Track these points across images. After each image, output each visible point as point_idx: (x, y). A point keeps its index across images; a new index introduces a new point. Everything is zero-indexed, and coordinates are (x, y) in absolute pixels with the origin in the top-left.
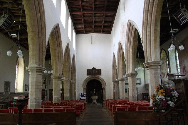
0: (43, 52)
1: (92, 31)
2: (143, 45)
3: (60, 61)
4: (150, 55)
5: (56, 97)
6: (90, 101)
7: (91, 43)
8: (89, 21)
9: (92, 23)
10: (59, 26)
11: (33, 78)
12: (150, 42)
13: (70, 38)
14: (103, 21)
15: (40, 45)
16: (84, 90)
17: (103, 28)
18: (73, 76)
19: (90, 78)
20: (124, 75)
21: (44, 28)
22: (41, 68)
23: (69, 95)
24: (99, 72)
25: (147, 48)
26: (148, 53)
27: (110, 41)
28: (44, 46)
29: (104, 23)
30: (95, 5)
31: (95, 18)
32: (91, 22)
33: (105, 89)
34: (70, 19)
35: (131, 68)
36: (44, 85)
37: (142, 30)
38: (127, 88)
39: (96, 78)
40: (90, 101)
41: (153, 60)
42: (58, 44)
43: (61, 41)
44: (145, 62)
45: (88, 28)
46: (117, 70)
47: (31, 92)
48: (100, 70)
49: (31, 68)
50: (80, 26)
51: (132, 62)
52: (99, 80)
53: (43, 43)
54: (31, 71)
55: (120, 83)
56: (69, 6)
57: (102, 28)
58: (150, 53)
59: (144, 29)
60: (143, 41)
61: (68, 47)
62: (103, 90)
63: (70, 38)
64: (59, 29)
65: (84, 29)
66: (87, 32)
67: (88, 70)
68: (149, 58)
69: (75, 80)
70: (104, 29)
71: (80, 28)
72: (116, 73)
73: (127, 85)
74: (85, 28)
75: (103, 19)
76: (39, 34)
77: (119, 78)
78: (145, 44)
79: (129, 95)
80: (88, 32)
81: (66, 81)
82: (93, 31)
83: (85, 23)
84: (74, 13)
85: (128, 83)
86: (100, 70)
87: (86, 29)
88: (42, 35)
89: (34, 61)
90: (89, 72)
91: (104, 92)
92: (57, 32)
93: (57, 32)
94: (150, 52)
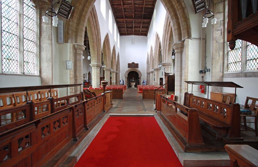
1: (132, 34)
3: (109, 58)
6: (130, 86)
7: (132, 44)
8: (130, 26)
9: (133, 27)
13: (116, 41)
16: (126, 78)
17: (141, 31)
18: (118, 68)
19: (130, 70)
20: (159, 65)
23: (115, 81)
24: (136, 65)
27: (146, 41)
29: (142, 28)
30: (134, 14)
33: (141, 78)
34: (115, 24)
39: (135, 70)
41: (166, 62)
42: (108, 47)
44: (162, 63)
45: (129, 31)
48: (138, 64)
50: (123, 29)
52: (137, 71)
55: (151, 74)
56: (114, 15)
60: (162, 49)
62: (140, 79)
63: (116, 41)
65: (126, 32)
66: (129, 34)
67: (129, 64)
68: (164, 60)
69: (119, 71)
71: (124, 30)
72: (148, 68)
74: (127, 31)
81: (107, 70)
82: (133, 34)
83: (127, 27)
84: (118, 20)
86: (138, 64)
87: (128, 32)
89: (95, 60)
90: (130, 65)
91: (140, 80)
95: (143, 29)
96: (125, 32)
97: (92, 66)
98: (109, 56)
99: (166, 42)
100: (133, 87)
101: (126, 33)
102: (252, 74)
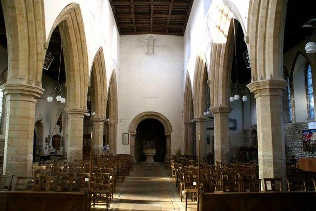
0: (37, 54)
2: (248, 46)
3: (82, 79)
4: (262, 67)
5: (72, 149)
6: (142, 158)
8: (145, 9)
10: (80, 10)
11: (224, 160)
12: (265, 38)
14: (170, 10)
15: (31, 40)
17: (170, 24)
20: (206, 111)
21: (38, 2)
22: (32, 87)
25: (256, 53)
26: (260, 63)
28: (41, 41)
31: (154, 4)
32: (147, 11)
33: (170, 136)
35: (220, 97)
36: (58, 127)
37: (247, 16)
38: (211, 136)
40: (142, 158)
42: (80, 47)
43: (85, 41)
46: (192, 101)
47: (9, 138)
49: (8, 88)
50: (127, 18)
51: (221, 85)
52: (160, 119)
53: (39, 36)
54: (10, 93)
57: (168, 23)
58: (262, 63)
59: (253, 12)
60: (248, 38)
61: (100, 55)
64: (81, 16)
65: (134, 25)
70: (172, 26)
73: (209, 131)
74: (137, 23)
75: (171, 6)
76: (27, 15)
77: (196, 117)
78: (254, 44)
79: (215, 149)
80: (142, 31)
82: (152, 31)
85: (212, 127)
87: (139, 25)
88: (35, 17)
92: (75, 22)
93: (75, 22)
94: (262, 61)
95: (174, 16)
96: (132, 25)
97: (69, 112)
98: (82, 73)
99: (262, 12)
100: (151, 160)
101: (133, 28)
102: (86, 140)
